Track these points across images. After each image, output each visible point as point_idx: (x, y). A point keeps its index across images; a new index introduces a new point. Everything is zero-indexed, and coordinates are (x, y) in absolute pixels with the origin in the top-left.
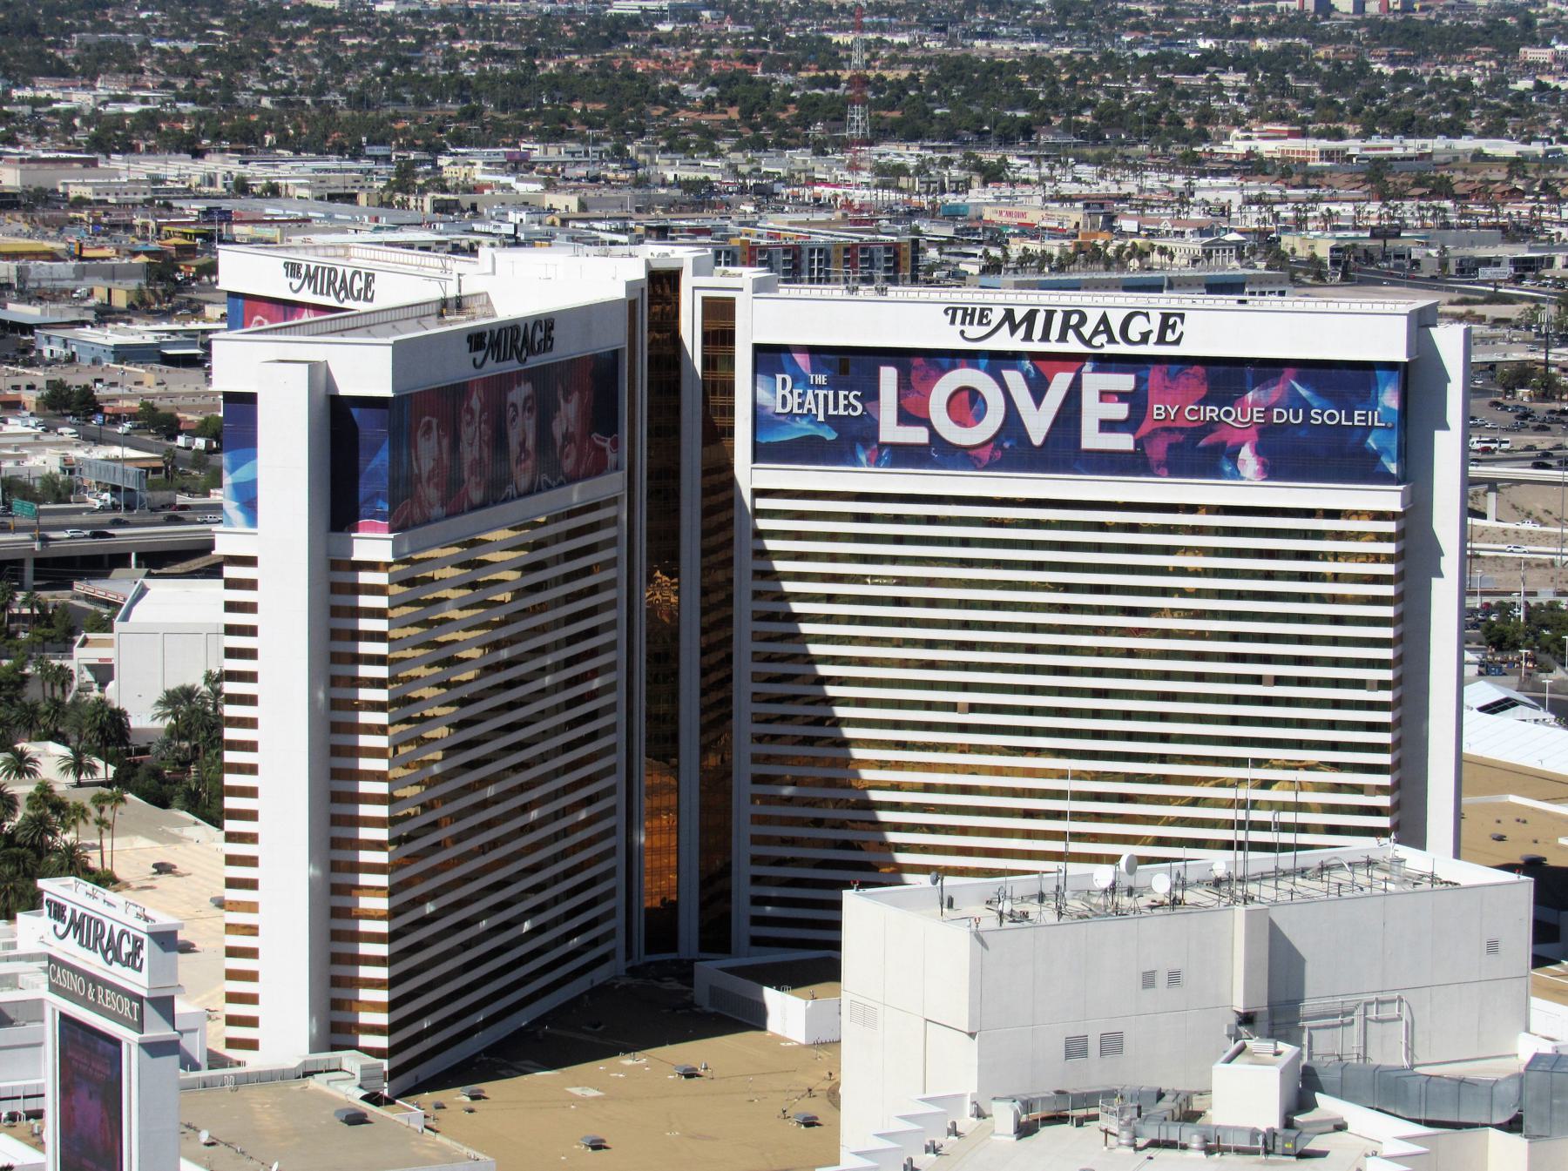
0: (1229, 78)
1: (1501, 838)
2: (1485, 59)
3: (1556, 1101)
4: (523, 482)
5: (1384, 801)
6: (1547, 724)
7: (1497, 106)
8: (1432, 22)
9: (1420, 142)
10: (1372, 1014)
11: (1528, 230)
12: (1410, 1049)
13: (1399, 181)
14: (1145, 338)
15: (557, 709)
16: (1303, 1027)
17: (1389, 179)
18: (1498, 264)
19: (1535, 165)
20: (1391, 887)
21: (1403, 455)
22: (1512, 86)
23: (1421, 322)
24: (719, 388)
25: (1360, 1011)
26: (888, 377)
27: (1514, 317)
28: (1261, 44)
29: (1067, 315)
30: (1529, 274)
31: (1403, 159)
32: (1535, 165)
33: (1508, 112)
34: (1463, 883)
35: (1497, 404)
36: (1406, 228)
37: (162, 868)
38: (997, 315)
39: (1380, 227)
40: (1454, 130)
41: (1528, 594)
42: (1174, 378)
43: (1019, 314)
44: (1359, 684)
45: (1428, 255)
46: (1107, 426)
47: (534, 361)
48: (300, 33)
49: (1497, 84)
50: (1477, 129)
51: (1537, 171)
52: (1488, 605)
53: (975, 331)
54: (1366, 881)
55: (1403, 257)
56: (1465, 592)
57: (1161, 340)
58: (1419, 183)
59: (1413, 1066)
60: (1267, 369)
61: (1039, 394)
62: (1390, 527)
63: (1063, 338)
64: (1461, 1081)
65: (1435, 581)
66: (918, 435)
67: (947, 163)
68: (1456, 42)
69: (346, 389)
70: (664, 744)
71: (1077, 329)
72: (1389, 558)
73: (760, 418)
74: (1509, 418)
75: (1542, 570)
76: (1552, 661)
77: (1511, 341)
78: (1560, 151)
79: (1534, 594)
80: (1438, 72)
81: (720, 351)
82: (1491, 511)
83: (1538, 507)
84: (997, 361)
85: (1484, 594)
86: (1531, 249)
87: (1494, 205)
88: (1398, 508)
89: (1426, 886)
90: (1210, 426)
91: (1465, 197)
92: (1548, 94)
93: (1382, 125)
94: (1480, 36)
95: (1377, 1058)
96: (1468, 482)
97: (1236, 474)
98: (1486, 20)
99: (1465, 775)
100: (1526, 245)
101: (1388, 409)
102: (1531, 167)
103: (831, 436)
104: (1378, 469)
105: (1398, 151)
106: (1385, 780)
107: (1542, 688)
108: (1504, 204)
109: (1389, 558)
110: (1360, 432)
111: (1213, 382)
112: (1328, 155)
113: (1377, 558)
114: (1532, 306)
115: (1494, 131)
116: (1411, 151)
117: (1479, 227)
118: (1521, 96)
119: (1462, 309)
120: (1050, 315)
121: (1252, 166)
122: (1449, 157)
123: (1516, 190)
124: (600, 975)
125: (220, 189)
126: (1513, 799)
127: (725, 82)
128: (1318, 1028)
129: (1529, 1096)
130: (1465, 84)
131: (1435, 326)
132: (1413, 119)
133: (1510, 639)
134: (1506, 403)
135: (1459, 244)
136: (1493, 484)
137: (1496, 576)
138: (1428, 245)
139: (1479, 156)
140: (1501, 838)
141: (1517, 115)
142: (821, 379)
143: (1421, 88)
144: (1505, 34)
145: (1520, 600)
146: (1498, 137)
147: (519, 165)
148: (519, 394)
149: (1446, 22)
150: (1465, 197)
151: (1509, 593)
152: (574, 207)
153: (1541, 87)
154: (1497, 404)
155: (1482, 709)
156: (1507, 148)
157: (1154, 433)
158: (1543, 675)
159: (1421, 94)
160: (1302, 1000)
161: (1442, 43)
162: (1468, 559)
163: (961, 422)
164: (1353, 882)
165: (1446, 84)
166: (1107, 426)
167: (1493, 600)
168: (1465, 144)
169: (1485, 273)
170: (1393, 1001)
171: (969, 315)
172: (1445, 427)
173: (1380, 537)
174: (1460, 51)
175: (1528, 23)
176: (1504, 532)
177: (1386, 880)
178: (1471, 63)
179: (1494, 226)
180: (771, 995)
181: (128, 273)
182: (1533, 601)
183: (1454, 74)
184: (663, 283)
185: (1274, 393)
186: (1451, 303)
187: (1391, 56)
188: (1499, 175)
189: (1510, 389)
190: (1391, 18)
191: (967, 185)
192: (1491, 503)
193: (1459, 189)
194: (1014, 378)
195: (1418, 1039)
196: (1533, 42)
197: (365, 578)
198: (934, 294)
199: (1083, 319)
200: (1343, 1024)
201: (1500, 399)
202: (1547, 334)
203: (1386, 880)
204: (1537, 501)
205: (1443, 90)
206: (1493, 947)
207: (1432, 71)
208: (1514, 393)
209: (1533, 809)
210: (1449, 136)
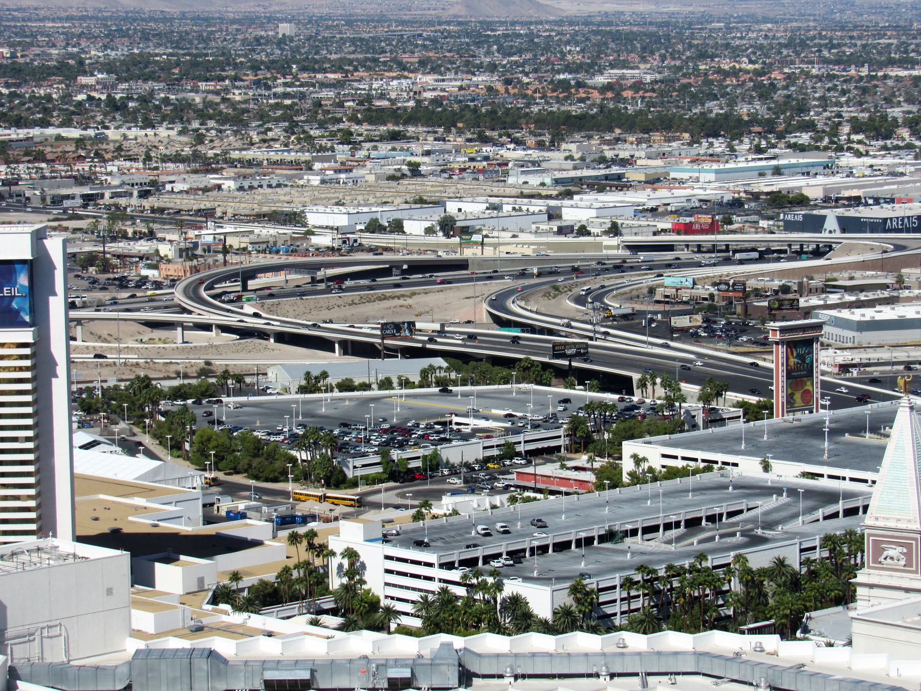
1: (96, 519)
2: (59, 83)
3: (149, 675)
5: (32, 503)
6: (118, 454)
7: (67, 110)
8: (27, 64)
9: (26, 131)
10: (45, 634)
11: (89, 178)
12: (67, 651)
13: (16, 153)
16: (7, 645)
17: (10, 152)
18: (73, 198)
19: (90, 142)
20: (52, 562)
21: (32, 311)
22: (74, 98)
23: (38, 237)
25: (38, 633)
27: (85, 227)
30: (91, 203)
31: (17, 141)
32: (90, 142)
33: (73, 113)
34: (92, 558)
35: (77, 276)
36: (21, 179)
39: (7, 179)
40: (45, 124)
41: (102, 381)
45: (35, 194)
49: (66, 98)
50: (57, 123)
51: (91, 145)
52: (81, 389)
54: (37, 560)
55: (20, 195)
56: (70, 383)
58: (27, 154)
59: (69, 661)
62: (27, 351)
64: (97, 668)
65: (54, 380)
68: (42, 74)
72: (27, 369)
74: (85, 284)
75: (109, 368)
76: (118, 419)
77: (83, 241)
78: (103, 133)
79: (106, 381)
80: (33, 92)
82: (79, 336)
83: (104, 333)
85: (78, 383)
86: (91, 189)
87: (69, 165)
88: (31, 340)
89: (71, 560)
91: (53, 161)
92: (94, 102)
93: (4, 122)
94: (55, 71)
95: (49, 658)
96: (68, 320)
98: (58, 62)
99: (76, 484)
100: (88, 187)
101: (22, 286)
102: (88, 143)
104: (19, 319)
105: (14, 137)
106: (32, 492)
107: (113, 434)
108: (75, 164)
109: (27, 369)
110: (8, 299)
113: (21, 369)
114: (94, 220)
115: (66, 124)
116: (21, 136)
117: (62, 177)
118: (80, 104)
119: (55, 224)
122: (43, 139)
123: (81, 156)
126: (102, 496)
128: (15, 644)
129: (134, 673)
130: (49, 98)
131: (46, 238)
132: (21, 118)
133: (94, 407)
134: (83, 275)
135: (51, 187)
136: (79, 321)
137: (84, 372)
138: (34, 189)
139: (59, 138)
140: (96, 519)
141: (78, 114)
143: (24, 101)
144: (69, 69)
145: (98, 385)
146: (69, 127)
149: (36, 63)
150: (53, 161)
151: (92, 382)
153: (90, 98)
154: (77, 276)
155: (81, 447)
156: (74, 133)
158: (113, 426)
159: (24, 104)
160: (6, 629)
161: (34, 75)
162: (70, 362)
164: (30, 562)
165: (38, 98)
167: (83, 386)
168: (51, 131)
169: (67, 203)
170: (56, 626)
172: (55, 294)
173: (22, 357)
174: (44, 79)
175: (81, 63)
176: (87, 347)
177: (49, 559)
178: (51, 86)
179: (70, 177)
182: (105, 385)
183: (42, 92)
186: (49, 221)
187: (6, 83)
188: (71, 148)
189: (84, 267)
190: (5, 62)
192: (78, 332)
193: (49, 157)
195: (71, 645)
196: (85, 73)
200: (29, 641)
201: (80, 273)
202: (104, 236)
203: (49, 559)
204: (103, 329)
205: (37, 101)
206: (109, 591)
207: (30, 91)
208: (87, 270)
209: (113, 502)
210: (42, 127)
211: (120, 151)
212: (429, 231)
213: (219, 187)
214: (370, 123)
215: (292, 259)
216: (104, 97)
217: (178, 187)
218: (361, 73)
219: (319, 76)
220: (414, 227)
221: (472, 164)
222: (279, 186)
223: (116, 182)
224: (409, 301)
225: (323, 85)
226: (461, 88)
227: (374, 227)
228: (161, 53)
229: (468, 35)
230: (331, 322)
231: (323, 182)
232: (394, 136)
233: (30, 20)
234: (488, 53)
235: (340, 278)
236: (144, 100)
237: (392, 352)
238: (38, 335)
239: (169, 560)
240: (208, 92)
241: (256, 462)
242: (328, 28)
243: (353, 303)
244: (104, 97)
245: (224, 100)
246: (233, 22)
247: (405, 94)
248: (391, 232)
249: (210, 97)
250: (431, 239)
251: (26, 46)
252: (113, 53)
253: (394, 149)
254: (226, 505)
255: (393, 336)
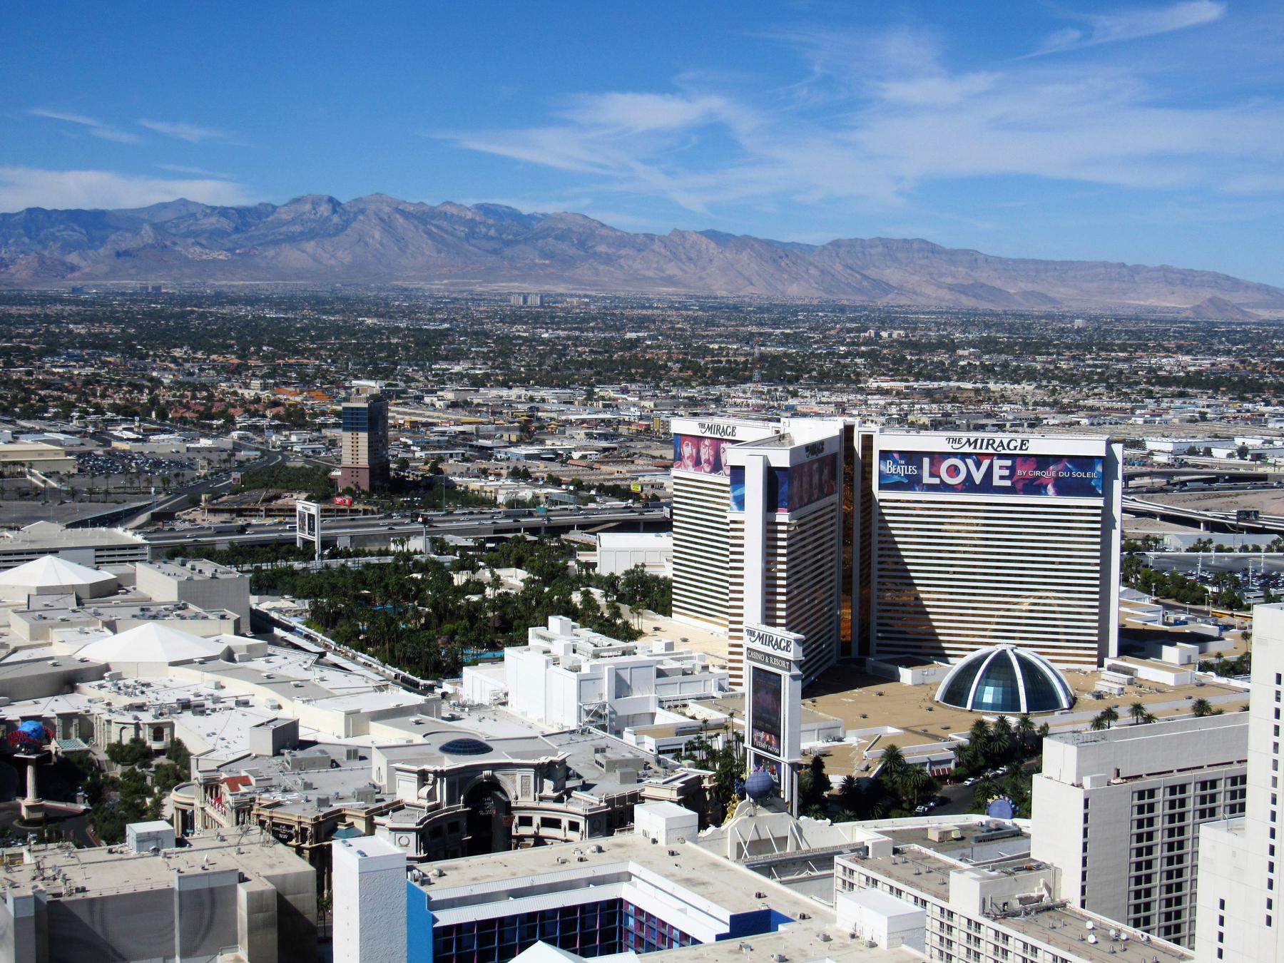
0: (858, 361)
4: (816, 496)
14: (1015, 448)
15: (809, 573)
21: (1103, 489)
23: (1109, 443)
24: (867, 466)
26: (926, 461)
28: (863, 348)
29: (989, 440)
37: (656, 629)
38: (964, 440)
42: (1025, 462)
43: (972, 441)
44: (1053, 563)
46: (1002, 478)
47: (820, 455)
48: (521, 345)
53: (957, 446)
57: (1021, 449)
60: (1057, 459)
61: (978, 467)
62: (1099, 511)
63: (987, 448)
66: (937, 481)
67: (776, 390)
68: (932, 347)
69: (773, 465)
70: (847, 589)
71: (992, 445)
73: (881, 475)
81: (867, 452)
84: (964, 456)
88: (1102, 505)
90: (1038, 478)
97: (1046, 494)
103: (906, 481)
111: (1038, 462)
112: (907, 388)
118: (963, 367)
120: (983, 440)
121: (880, 391)
124: (830, 663)
125: (523, 400)
127: (683, 361)
139: (959, 388)
142: (903, 462)
147: (625, 391)
148: (816, 466)
152: (652, 406)
157: (1018, 480)
163: (951, 476)
166: (1002, 478)
168: (952, 384)
171: (954, 440)
180: (902, 671)
181: (514, 429)
184: (848, 430)
185: (1060, 466)
191: (787, 399)
194: (969, 461)
197: (780, 528)
198: (945, 433)
199: (994, 442)
211: (1005, 399)
212: (1230, 456)
213: (1078, 423)
214: (1161, 386)
215: (1144, 469)
216: (978, 363)
217: (1052, 422)
218: (1139, 353)
219: (1113, 354)
220: (1220, 453)
221: (1240, 414)
222: (1116, 423)
223: (1010, 417)
224: (1235, 499)
225: (1118, 360)
226: (1213, 365)
227: (1192, 451)
228: (1003, 337)
229: (1202, 330)
230: (1207, 510)
231: (1145, 422)
232: (1181, 395)
233: (908, 313)
234: (1220, 343)
235: (1184, 483)
236: (1005, 365)
237: (1241, 530)
238: (1105, 502)
239: (1172, 644)
240: (1043, 362)
241: (1182, 592)
242: (1106, 323)
243: (1199, 499)
244: (978, 363)
245: (1057, 368)
246: (1042, 318)
247: (1176, 368)
248: (1204, 455)
249: (1047, 366)
250: (1232, 461)
251: (915, 329)
252: (970, 336)
253: (1185, 403)
254: (1172, 617)
255: (1244, 520)
